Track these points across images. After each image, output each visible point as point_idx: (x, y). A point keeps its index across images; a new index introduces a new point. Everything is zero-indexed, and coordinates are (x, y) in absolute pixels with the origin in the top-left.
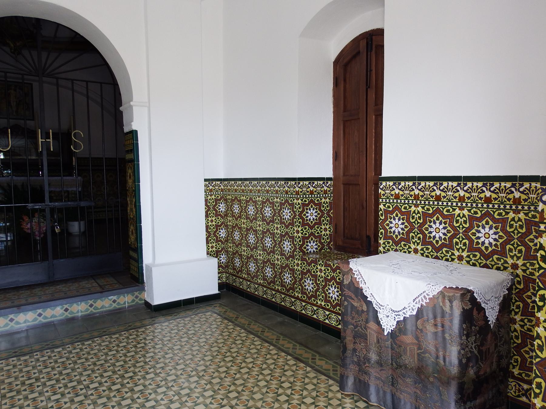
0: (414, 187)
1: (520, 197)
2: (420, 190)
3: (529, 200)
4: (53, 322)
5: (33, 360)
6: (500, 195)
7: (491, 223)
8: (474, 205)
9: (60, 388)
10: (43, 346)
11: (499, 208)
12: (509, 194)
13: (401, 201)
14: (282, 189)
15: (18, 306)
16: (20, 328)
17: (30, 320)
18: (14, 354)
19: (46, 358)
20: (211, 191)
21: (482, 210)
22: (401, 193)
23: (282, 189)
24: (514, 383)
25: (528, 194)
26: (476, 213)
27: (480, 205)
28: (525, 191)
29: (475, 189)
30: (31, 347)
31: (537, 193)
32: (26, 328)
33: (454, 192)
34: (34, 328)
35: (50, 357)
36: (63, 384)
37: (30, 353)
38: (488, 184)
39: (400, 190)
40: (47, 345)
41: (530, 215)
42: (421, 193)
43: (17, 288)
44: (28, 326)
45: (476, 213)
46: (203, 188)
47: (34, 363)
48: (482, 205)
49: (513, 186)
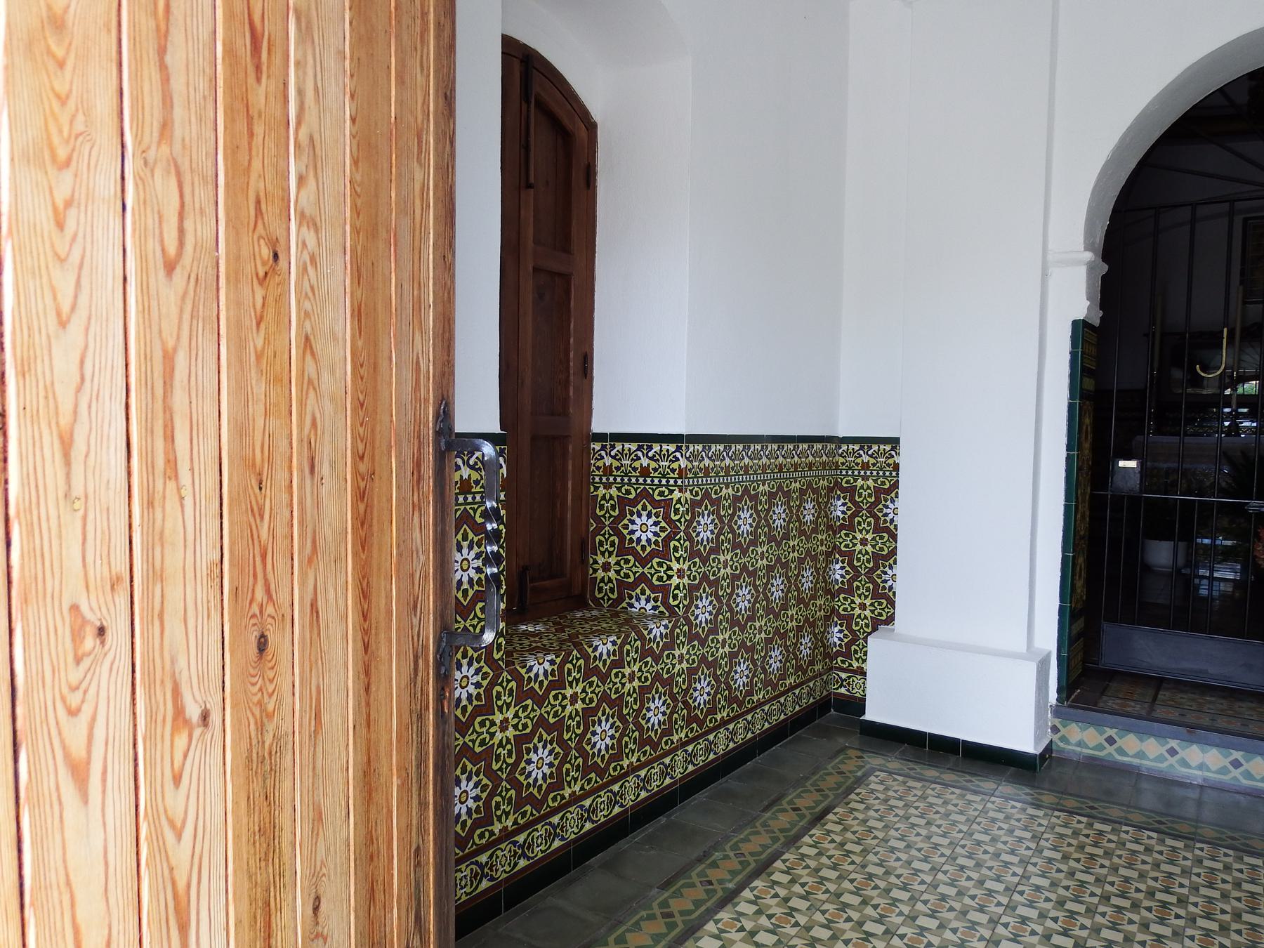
0: (603, 453)
2: (613, 457)
4: (1138, 767)
5: (1189, 855)
8: (626, 479)
9: (1131, 922)
10: (1224, 837)
13: (474, 498)
14: (696, 464)
15: (1191, 727)
16: (1188, 778)
17: (1214, 768)
18: (1157, 825)
19: (1220, 866)
22: (653, 465)
23: (696, 464)
27: (634, 480)
30: (1196, 827)
32: (1200, 781)
34: (1220, 788)
35: (1227, 868)
36: (1142, 918)
37: (1190, 839)
39: (651, 458)
40: (1233, 838)
42: (616, 464)
43: (1203, 689)
44: (1205, 780)
47: (1188, 863)
49: (640, 448)
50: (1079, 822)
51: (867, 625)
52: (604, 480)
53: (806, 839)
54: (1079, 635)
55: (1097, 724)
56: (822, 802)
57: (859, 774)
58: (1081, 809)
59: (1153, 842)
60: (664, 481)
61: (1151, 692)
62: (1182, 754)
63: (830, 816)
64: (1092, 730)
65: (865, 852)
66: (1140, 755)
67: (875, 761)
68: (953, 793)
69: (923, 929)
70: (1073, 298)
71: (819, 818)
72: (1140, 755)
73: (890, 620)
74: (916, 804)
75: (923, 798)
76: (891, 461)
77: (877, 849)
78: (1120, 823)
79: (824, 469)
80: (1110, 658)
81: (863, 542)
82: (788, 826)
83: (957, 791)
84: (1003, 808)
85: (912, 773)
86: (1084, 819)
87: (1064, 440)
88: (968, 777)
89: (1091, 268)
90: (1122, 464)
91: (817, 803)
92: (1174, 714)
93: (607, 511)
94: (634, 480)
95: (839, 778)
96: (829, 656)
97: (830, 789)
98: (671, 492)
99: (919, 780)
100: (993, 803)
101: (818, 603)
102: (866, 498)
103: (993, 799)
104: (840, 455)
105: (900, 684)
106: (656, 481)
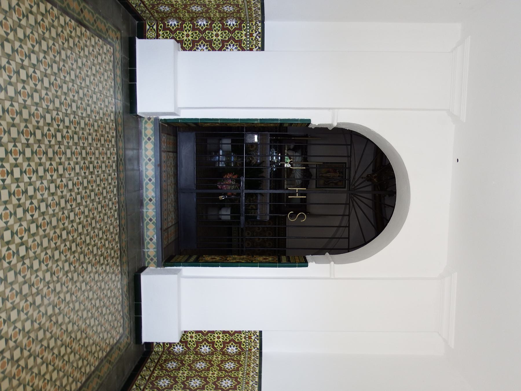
4: (141, 149)
8: (248, 42)
15: (160, 166)
20: (250, 338)
27: (248, 46)
32: (141, 169)
43: (176, 166)
45: (244, 44)
46: (252, 329)
49: (257, 336)
50: (113, 133)
51: (179, 38)
52: (248, 34)
53: (68, 19)
54: (189, 126)
55: (155, 134)
56: (89, 23)
57: (109, 40)
58: (119, 132)
59: (112, 159)
61: (171, 150)
62: (150, 163)
63: (84, 29)
64: (152, 132)
65: (71, 49)
66: (146, 150)
67: (118, 47)
68: (111, 83)
69: (42, 81)
70: (318, 120)
71: (81, 23)
72: (146, 150)
73: (184, 49)
74: (101, 68)
75: (106, 71)
76: (254, 47)
77: (74, 54)
78: (117, 147)
79: (249, 15)
80: (182, 136)
81: (217, 35)
82: (72, 8)
83: (113, 84)
84: (112, 102)
85: (116, 63)
86: (115, 134)
87: (264, 118)
88: (120, 88)
89: (330, 125)
90: (256, 137)
91: (89, 21)
92: (164, 159)
93: (217, 45)
94: (248, 46)
95: (104, 30)
96: (162, 20)
97: (97, 27)
99: (114, 67)
100: (112, 99)
101: (186, 14)
102: (237, 35)
103: (113, 100)
104: (256, 23)
105: (155, 55)
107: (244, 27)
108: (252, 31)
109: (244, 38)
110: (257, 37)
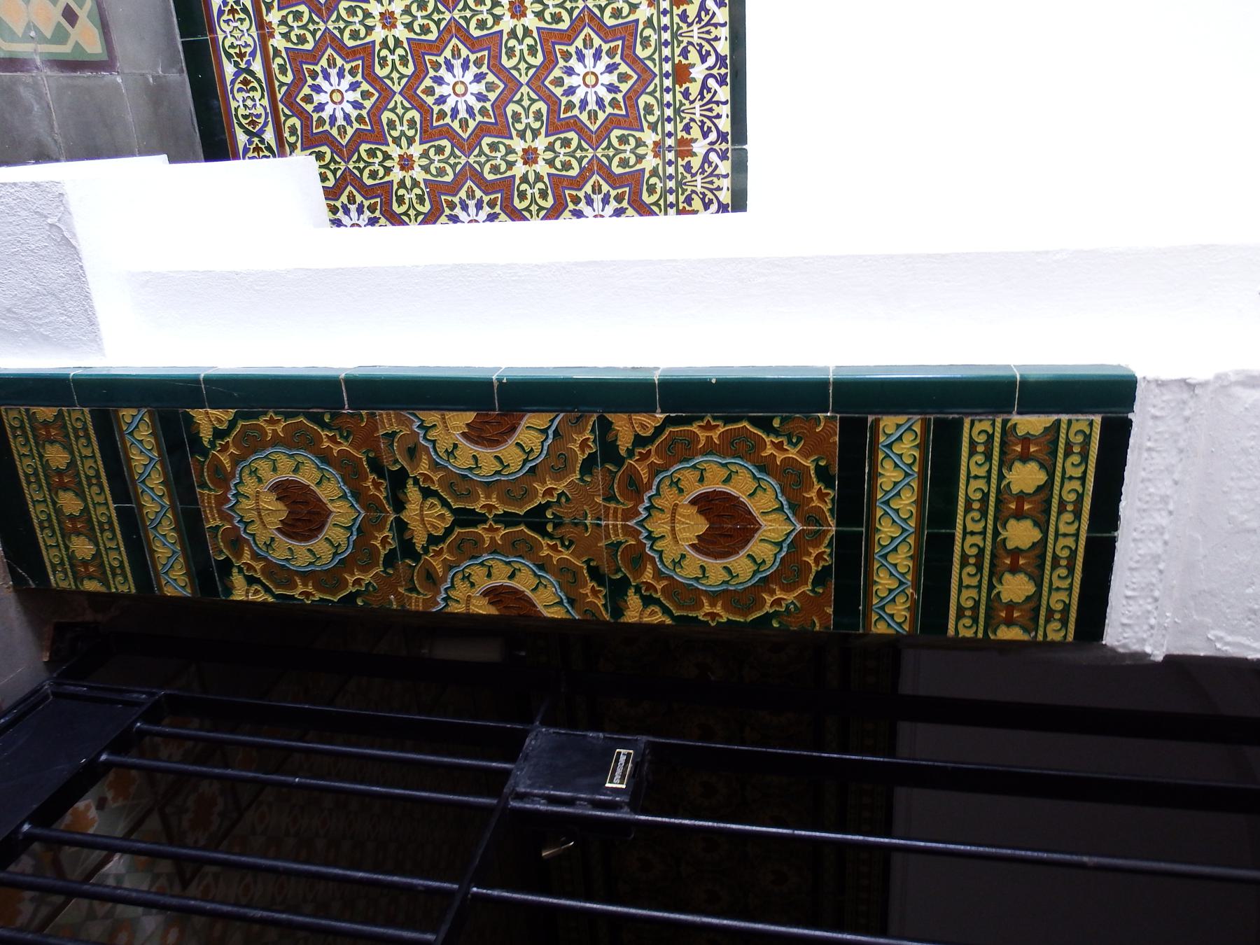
1: (694, 154)
3: (688, 176)
6: (697, 104)
7: (624, 87)
8: (666, 36)
11: (663, 105)
12: (702, 128)
21: (653, 60)
24: (224, 25)
25: (704, 171)
26: (646, 42)
27: (666, 52)
28: (710, 164)
29: (711, 110)
31: (704, 43)
33: (703, 123)
38: (723, 71)
41: (648, 32)
45: (646, 42)
48: (667, 59)
49: (720, 59)
60: (669, 112)
94: (666, 52)
98: (653, 127)
106: (668, 97)
107: (649, 109)
108: (687, 128)
109: (650, 163)
110: (713, 157)
